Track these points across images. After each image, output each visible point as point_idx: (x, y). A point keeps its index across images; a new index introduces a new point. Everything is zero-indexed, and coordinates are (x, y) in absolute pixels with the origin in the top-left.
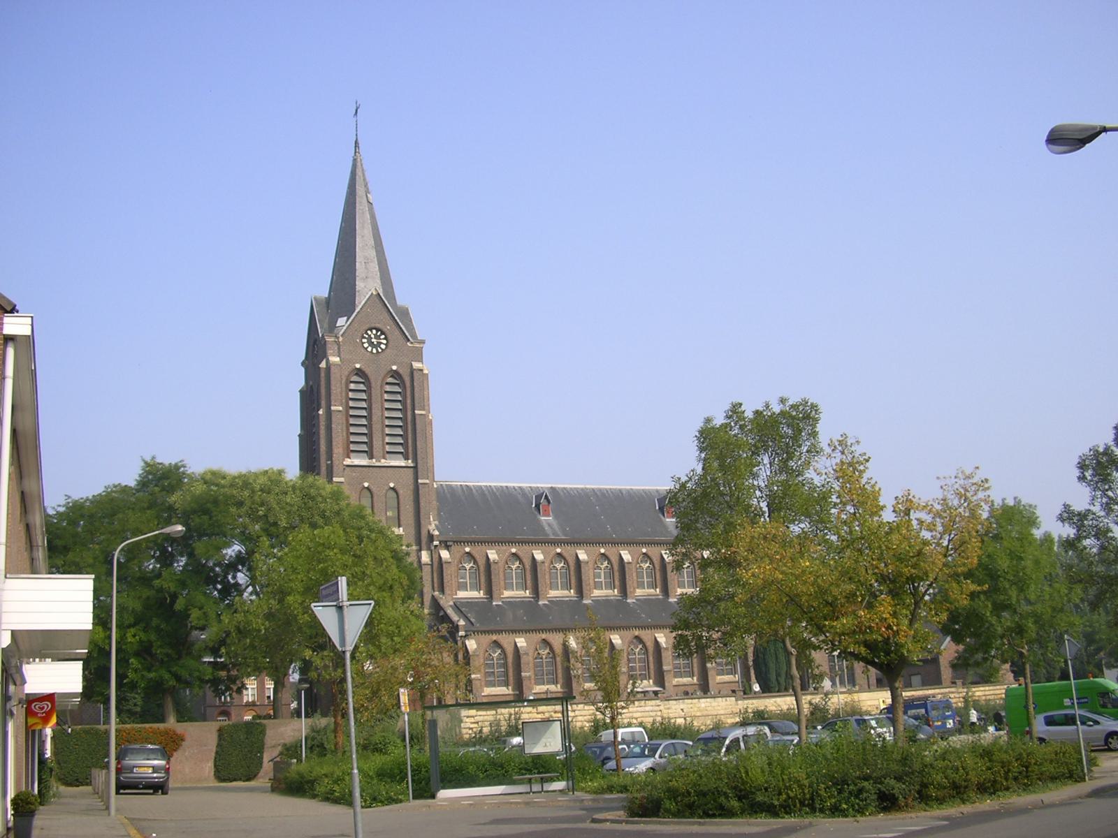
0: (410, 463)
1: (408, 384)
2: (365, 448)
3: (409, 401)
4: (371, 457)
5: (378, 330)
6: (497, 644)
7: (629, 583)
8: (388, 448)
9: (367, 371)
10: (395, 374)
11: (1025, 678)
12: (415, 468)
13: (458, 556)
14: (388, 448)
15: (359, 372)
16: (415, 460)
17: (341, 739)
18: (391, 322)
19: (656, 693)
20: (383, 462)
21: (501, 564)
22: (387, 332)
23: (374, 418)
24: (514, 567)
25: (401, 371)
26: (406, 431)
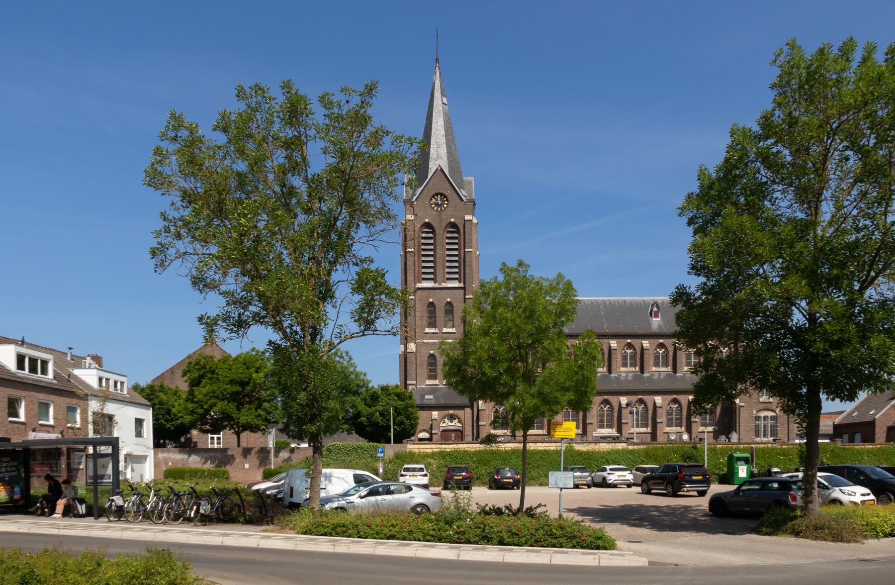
0: (462, 285)
1: (462, 231)
2: (432, 276)
3: (462, 243)
4: (435, 282)
5: (433, 197)
6: (641, 401)
7: (613, 363)
8: (448, 276)
9: (433, 224)
10: (453, 225)
11: (498, 436)
12: (464, 288)
13: (623, 345)
14: (448, 276)
15: (428, 225)
16: (464, 284)
17: (660, 453)
18: (451, 188)
19: (618, 438)
20: (444, 285)
21: (652, 351)
22: (448, 196)
23: (438, 256)
24: (661, 352)
25: (457, 223)
26: (460, 264)
